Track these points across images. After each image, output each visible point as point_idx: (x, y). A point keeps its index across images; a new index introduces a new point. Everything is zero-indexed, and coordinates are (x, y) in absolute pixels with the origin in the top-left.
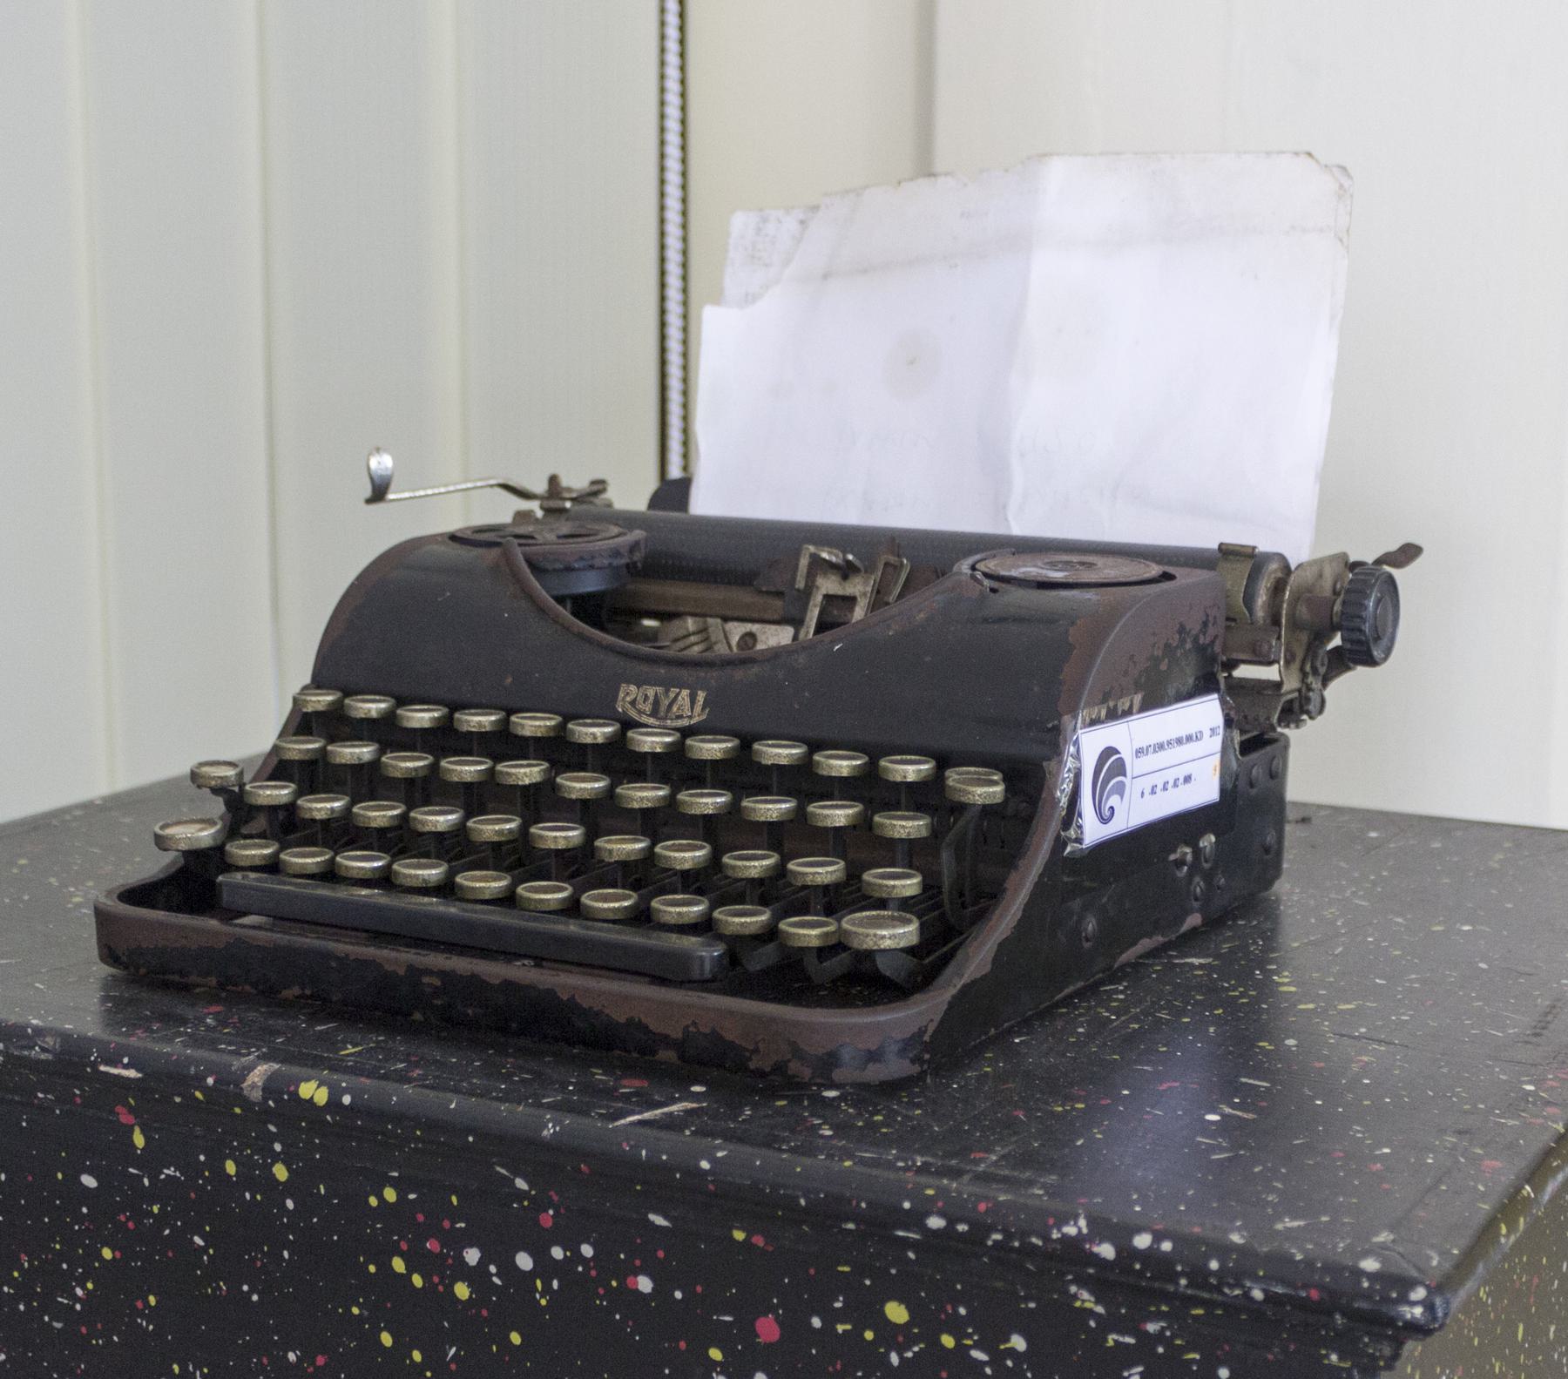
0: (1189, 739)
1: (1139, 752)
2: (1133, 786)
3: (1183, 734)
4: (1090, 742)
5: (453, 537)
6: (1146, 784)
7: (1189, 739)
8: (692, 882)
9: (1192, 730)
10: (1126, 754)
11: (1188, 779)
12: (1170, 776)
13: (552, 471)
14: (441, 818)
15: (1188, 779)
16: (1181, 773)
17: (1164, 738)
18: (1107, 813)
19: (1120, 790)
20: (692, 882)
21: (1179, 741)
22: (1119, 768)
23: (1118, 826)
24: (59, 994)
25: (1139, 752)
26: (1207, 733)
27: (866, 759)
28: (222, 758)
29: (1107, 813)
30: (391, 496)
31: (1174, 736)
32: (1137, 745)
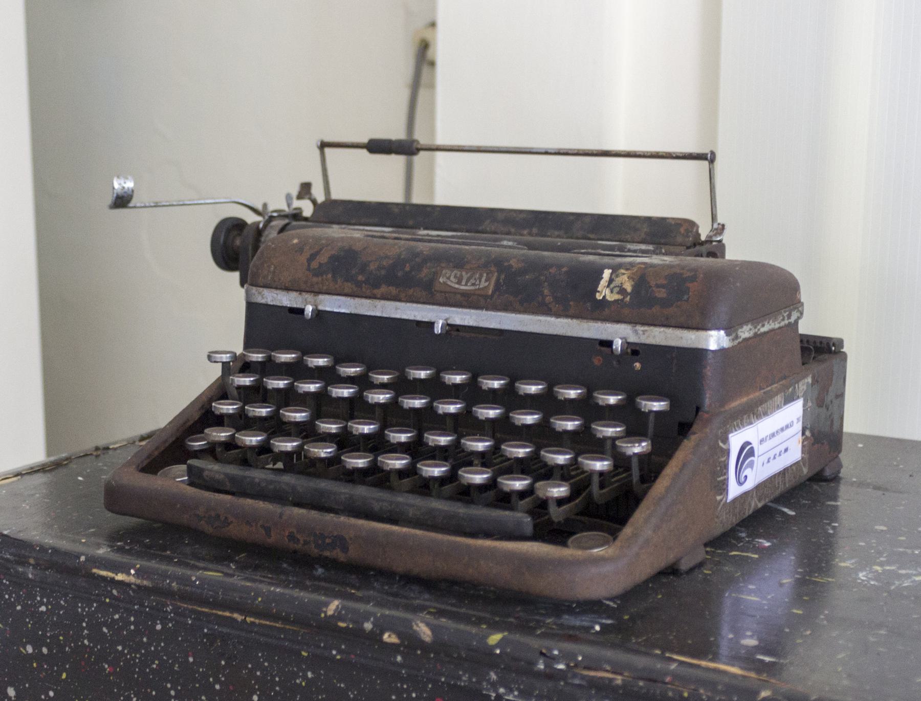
0: (787, 427)
1: (762, 441)
2: (757, 460)
3: (784, 425)
4: (736, 441)
5: (18, 474)
6: (764, 458)
7: (787, 427)
8: (484, 460)
9: (788, 422)
10: (755, 444)
11: (786, 450)
12: (777, 451)
13: (306, 180)
14: (298, 415)
15: (786, 450)
16: (782, 447)
17: (774, 430)
18: (742, 479)
19: (751, 465)
20: (484, 460)
21: (782, 430)
22: (751, 453)
23: (749, 485)
24: (28, 522)
25: (762, 441)
26: (795, 421)
27: (585, 390)
28: (241, 201)
29: (742, 479)
30: (131, 205)
31: (779, 427)
32: (760, 438)
